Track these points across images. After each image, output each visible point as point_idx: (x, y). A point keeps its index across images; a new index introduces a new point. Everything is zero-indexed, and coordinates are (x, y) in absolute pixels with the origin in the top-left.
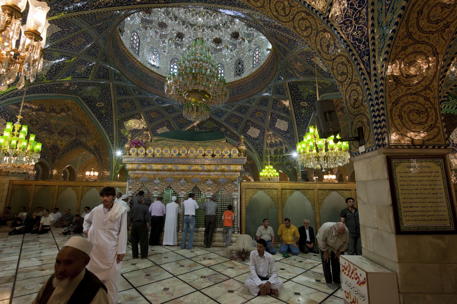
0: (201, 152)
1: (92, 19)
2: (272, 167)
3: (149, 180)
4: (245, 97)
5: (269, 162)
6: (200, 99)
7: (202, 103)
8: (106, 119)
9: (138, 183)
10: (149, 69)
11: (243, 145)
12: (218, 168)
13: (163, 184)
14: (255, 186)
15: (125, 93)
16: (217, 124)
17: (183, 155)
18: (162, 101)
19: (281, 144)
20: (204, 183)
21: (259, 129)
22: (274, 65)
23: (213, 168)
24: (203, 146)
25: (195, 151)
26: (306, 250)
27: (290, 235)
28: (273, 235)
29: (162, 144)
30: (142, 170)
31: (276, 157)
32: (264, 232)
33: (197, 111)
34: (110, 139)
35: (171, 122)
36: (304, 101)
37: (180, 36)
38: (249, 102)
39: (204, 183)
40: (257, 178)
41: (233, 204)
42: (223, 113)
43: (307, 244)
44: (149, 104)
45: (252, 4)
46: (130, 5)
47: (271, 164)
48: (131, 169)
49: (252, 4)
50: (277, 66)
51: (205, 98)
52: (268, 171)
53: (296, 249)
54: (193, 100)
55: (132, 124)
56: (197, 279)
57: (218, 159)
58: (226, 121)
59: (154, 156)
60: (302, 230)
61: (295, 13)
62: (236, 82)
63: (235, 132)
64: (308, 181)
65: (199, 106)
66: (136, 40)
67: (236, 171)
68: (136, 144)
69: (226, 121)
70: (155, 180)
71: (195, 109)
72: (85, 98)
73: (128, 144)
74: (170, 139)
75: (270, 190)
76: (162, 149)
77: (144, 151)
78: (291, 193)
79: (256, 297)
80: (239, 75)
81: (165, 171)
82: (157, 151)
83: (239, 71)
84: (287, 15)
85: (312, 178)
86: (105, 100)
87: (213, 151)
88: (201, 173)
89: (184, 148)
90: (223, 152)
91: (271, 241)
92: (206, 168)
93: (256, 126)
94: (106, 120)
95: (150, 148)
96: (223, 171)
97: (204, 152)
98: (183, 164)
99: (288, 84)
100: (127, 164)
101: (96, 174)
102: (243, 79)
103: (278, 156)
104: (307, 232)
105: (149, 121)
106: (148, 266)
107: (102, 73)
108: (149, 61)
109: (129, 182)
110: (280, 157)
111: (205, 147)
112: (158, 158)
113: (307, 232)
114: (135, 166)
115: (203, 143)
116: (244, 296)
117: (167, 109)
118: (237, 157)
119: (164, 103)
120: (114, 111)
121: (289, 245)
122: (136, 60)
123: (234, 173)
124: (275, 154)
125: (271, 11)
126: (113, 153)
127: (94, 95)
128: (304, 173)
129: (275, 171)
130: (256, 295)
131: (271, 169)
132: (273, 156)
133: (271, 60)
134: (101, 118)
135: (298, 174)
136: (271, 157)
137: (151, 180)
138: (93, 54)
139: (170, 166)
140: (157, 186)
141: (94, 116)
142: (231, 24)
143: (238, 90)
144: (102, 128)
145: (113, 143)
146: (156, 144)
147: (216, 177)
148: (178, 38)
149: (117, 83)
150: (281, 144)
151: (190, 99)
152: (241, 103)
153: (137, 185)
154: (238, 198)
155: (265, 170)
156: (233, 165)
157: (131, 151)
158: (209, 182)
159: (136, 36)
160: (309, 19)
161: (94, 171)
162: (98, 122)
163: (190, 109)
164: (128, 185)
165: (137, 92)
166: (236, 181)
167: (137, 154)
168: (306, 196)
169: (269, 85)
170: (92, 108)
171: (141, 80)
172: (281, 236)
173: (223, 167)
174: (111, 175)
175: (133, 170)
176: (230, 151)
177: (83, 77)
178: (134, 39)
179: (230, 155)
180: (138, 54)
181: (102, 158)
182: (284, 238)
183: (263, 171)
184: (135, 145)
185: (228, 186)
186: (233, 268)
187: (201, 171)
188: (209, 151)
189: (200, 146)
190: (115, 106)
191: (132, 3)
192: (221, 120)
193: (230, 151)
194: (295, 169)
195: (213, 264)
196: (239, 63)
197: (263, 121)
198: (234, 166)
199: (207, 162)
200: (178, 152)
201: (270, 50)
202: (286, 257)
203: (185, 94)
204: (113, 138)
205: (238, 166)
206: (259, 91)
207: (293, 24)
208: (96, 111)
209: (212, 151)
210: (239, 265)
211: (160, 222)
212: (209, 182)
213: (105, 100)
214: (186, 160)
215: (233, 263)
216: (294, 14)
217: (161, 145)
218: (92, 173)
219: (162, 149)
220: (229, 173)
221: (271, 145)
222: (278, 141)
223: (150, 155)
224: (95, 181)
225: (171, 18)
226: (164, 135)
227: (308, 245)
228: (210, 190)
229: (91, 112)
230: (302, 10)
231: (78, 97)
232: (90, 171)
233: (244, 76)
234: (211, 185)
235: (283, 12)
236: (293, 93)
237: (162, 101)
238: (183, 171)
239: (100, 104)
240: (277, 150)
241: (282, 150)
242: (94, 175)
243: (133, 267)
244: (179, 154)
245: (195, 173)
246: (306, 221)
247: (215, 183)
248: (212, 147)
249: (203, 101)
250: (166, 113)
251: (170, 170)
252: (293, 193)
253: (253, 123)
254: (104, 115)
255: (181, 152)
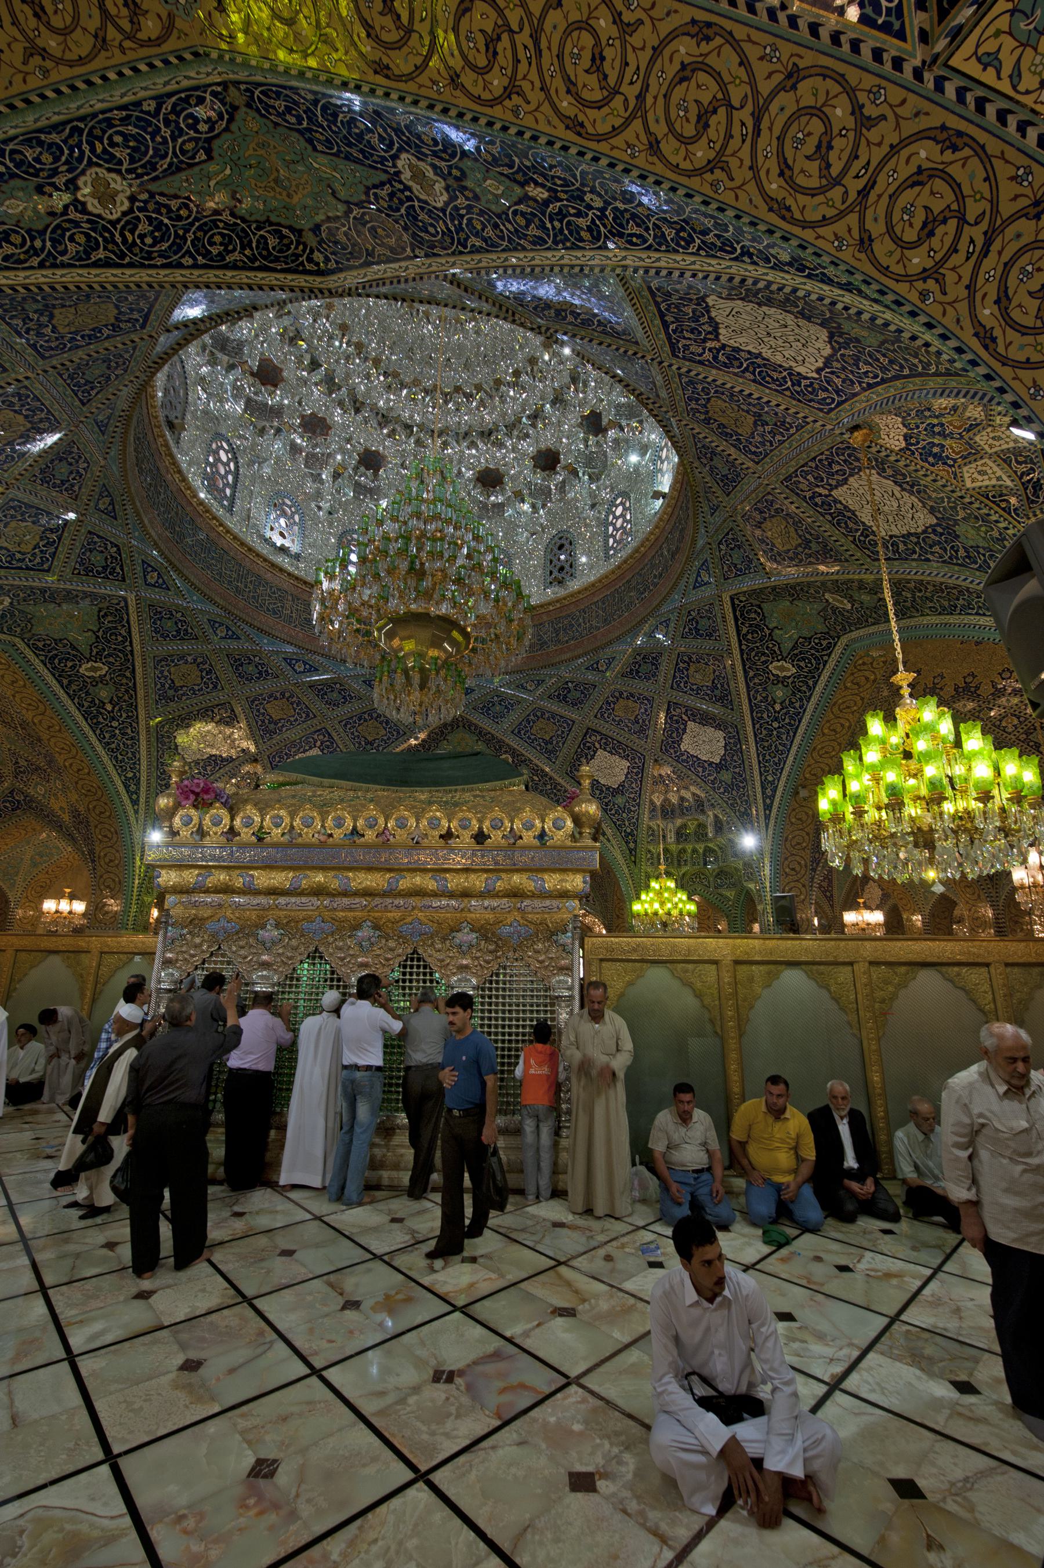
0: (434, 823)
1: (41, 326)
2: (671, 884)
3: (241, 930)
4: (580, 651)
5: (662, 867)
6: (437, 644)
7: (443, 656)
8: (113, 719)
9: (198, 940)
10: (265, 560)
11: (589, 801)
12: (499, 885)
13: (294, 942)
14: (635, 950)
15: (183, 634)
16: (487, 742)
17: (370, 835)
18: (305, 663)
19: (700, 806)
20: (444, 939)
21: (626, 757)
22: (681, 539)
23: (478, 882)
24: (444, 805)
25: (412, 822)
26: (850, 1207)
27: (783, 1145)
28: (715, 1145)
29: (294, 797)
30: (217, 890)
31: (685, 850)
32: (679, 1133)
33: (423, 686)
34: (126, 787)
35: (334, 734)
36: (784, 659)
37: (371, 461)
38: (594, 668)
39: (444, 939)
40: (617, 918)
41: (553, 1019)
42: (508, 704)
43: (846, 1182)
44: (263, 674)
45: (667, 164)
46: (180, 266)
47: (669, 874)
48: (173, 887)
49: (667, 164)
50: (694, 541)
51: (453, 643)
52: (661, 899)
53: (810, 1208)
54: (409, 646)
55: (199, 737)
56: (416, 1389)
57: (499, 848)
58: (517, 732)
59: (260, 839)
60: (822, 1122)
61: (878, 154)
62: (549, 604)
63: (547, 769)
64: (796, 931)
65: (429, 670)
66: (227, 464)
67: (564, 895)
68: (197, 794)
69: (517, 732)
70: (263, 927)
71: (416, 679)
72: (40, 645)
73: (169, 796)
74: (326, 781)
75: (690, 966)
76: (292, 815)
77: (226, 821)
78: (770, 979)
79: (711, 1524)
80: (560, 582)
81: (302, 893)
82: (277, 824)
83: (559, 572)
84: (837, 182)
85: (810, 922)
86: (109, 655)
87: (480, 821)
88: (436, 903)
89: (372, 810)
90: (518, 825)
91: (709, 1169)
92: (454, 882)
93: (617, 748)
94: (115, 724)
95: (250, 810)
96: (515, 894)
97: (445, 823)
98: (370, 869)
99: (732, 599)
100: (162, 867)
101: (79, 907)
102: (572, 595)
103: (689, 848)
104: (844, 1129)
105: (263, 728)
106: (203, 1305)
107: (97, 559)
108: (268, 534)
109: (165, 937)
110: (694, 851)
111: (451, 808)
112: (275, 845)
113: (844, 1129)
114: (190, 877)
115: (441, 794)
116: (654, 1516)
117: (321, 690)
118: (569, 843)
119: (313, 670)
120: (141, 693)
121: (778, 1188)
122: (221, 525)
123: (555, 903)
124: (678, 842)
125: (756, 178)
126: (137, 835)
127: (72, 635)
128: (783, 902)
129: (684, 897)
130: (711, 1510)
131: (668, 889)
132: (673, 848)
133: (668, 528)
134: (95, 717)
135: (760, 908)
136: (666, 850)
137: (247, 930)
138: (63, 483)
139: (320, 878)
140: (268, 950)
141: (73, 709)
142: (534, 426)
143: (557, 632)
144: (99, 749)
145: (135, 802)
146: (274, 796)
147: (490, 916)
148: (362, 469)
149: (155, 595)
150: (700, 806)
151: (396, 642)
152: (565, 673)
153: (196, 946)
154: (571, 997)
155: (651, 895)
156: (554, 871)
157: (177, 821)
158: (466, 936)
159: (227, 452)
160: (954, 170)
161: (72, 897)
162: (87, 729)
163: (400, 679)
164: (159, 946)
165: (222, 632)
166: (565, 932)
167: (201, 832)
168: (827, 988)
169: (664, 609)
170: (65, 682)
171: (238, 590)
172: (743, 1145)
173: (516, 878)
174: (126, 911)
175: (181, 892)
176: (543, 821)
177: (28, 568)
178: (218, 460)
179: (542, 835)
180: (230, 510)
181: (100, 855)
182: (757, 1155)
183: (643, 896)
184: (192, 797)
185: (537, 952)
186: (568, 1313)
187: (435, 895)
188: (465, 822)
189: (430, 803)
190: (145, 676)
191: (187, 261)
192: (502, 730)
193: (543, 821)
194: (748, 892)
195: (485, 1288)
196: (561, 547)
197: (642, 731)
198: (557, 876)
199: (458, 860)
200: (349, 824)
201: (664, 496)
202: (780, 1246)
203: (380, 630)
204: (138, 784)
205: (570, 877)
206: (629, 631)
207: (862, 221)
208: (78, 688)
209: (474, 822)
210: (597, 1296)
211: (260, 1099)
212: (466, 936)
213: (109, 655)
214: (380, 855)
215: (568, 1284)
216: (874, 164)
217: (290, 801)
218: (64, 906)
219: (292, 815)
220: (537, 903)
221: (667, 812)
222: (688, 795)
223: (246, 835)
224: (78, 931)
225: (341, 404)
226: (312, 768)
227: (855, 1186)
228: (466, 967)
229: (61, 693)
230: (924, 123)
231: (17, 640)
232: (58, 896)
233: (574, 585)
234: (471, 946)
235: (813, 167)
236: (745, 630)
237: (305, 663)
238: (367, 893)
239: (93, 669)
240: (684, 826)
241: (702, 826)
242: (70, 912)
243: (137, 1316)
244: (355, 831)
245: (413, 901)
246: (839, 1086)
247: (487, 939)
248: (474, 807)
249: (445, 650)
250: (317, 705)
251: (318, 892)
252: (776, 976)
253: (606, 737)
254: (109, 707)
255: (360, 823)
